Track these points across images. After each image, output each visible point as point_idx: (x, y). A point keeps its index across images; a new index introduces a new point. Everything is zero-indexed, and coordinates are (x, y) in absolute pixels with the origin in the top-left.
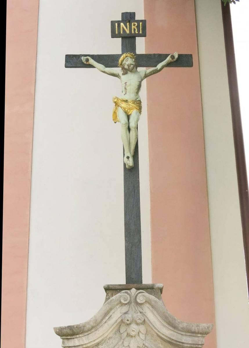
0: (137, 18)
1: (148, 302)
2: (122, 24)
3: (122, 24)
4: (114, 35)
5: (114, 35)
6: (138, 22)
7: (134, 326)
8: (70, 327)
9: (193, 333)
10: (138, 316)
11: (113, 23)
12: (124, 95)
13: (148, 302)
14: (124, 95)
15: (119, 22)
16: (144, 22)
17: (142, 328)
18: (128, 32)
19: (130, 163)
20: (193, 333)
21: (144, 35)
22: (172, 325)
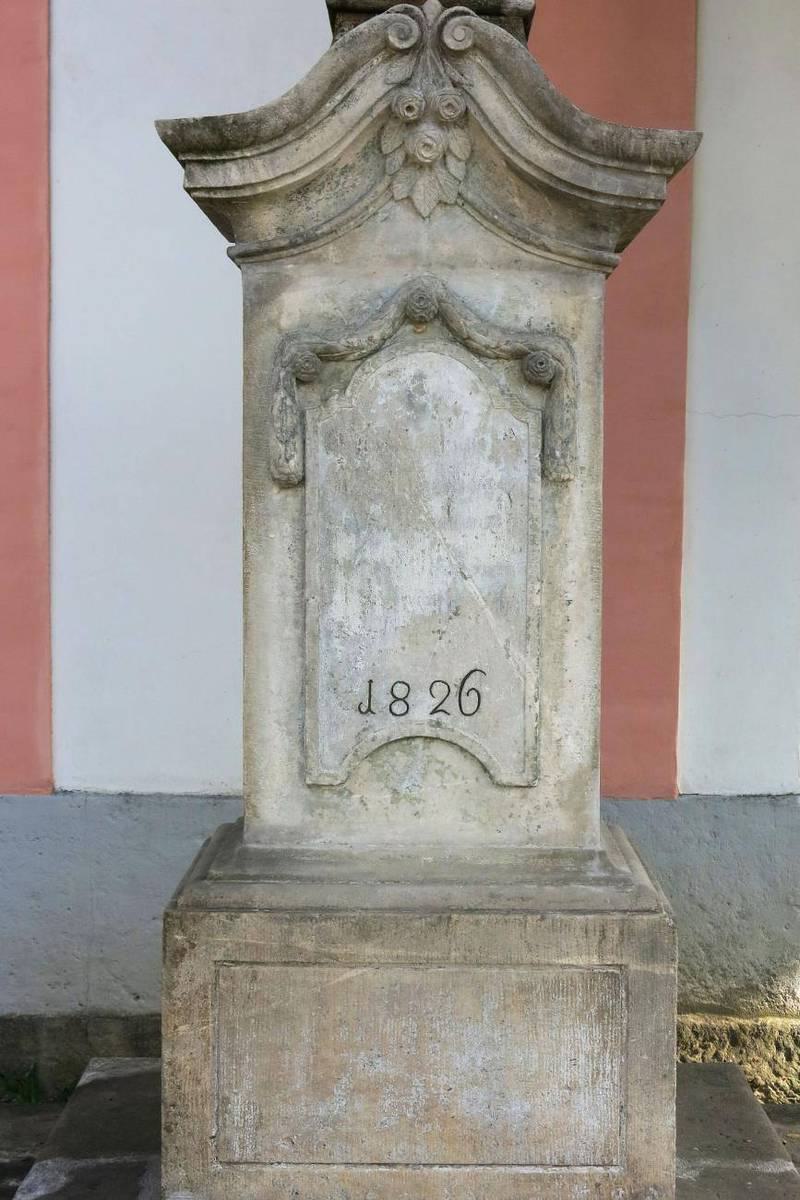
1: (481, 47)
7: (429, 131)
8: (211, 123)
9: (626, 159)
10: (444, 96)
13: (481, 47)
17: (458, 142)
20: (626, 159)
22: (559, 128)
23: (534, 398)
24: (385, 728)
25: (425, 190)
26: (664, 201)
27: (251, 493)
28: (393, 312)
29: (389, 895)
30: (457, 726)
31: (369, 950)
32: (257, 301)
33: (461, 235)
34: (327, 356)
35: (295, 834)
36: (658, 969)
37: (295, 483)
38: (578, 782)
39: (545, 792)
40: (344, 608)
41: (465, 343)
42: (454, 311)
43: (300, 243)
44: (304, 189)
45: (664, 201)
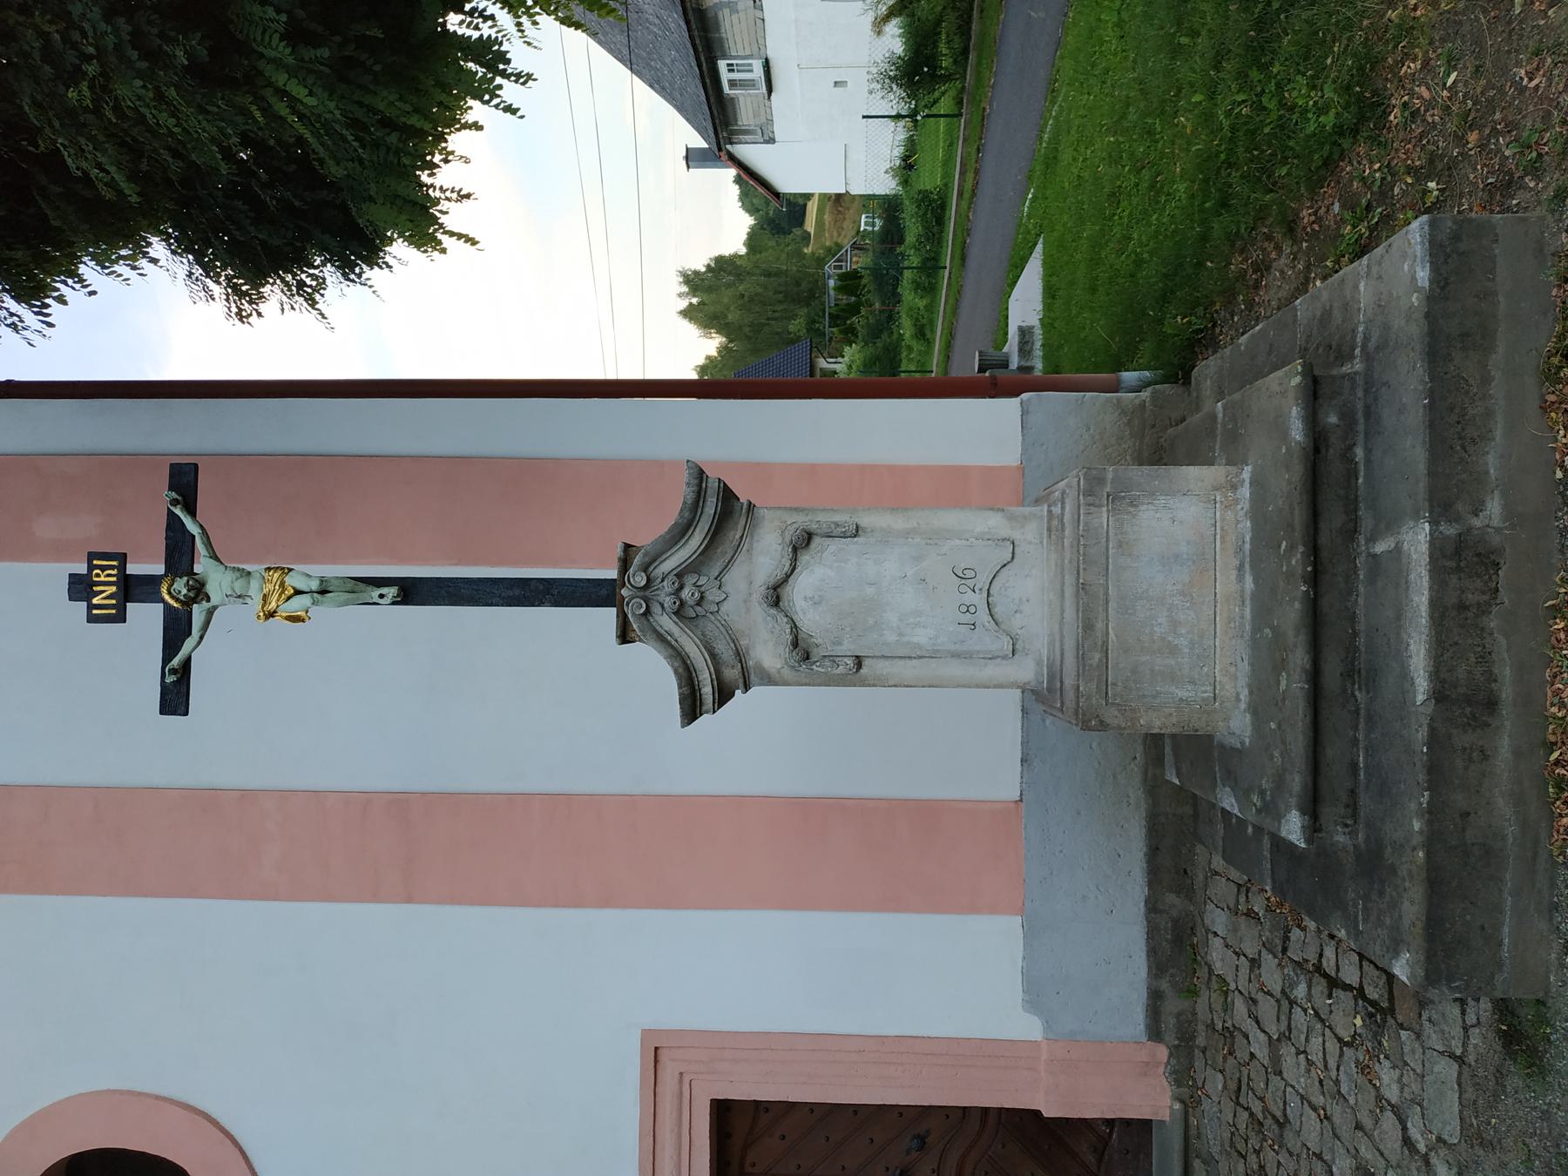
0: (82, 568)
2: (95, 601)
3: (95, 601)
4: (120, 617)
5: (120, 617)
6: (91, 567)
11: (92, 619)
12: (175, 698)
13: (645, 568)
14: (175, 698)
15: (91, 607)
16: (91, 556)
18: (114, 589)
19: (391, 592)
21: (123, 558)
23: (816, 541)
24: (983, 616)
25: (713, 595)
26: (692, 709)
27: (863, 683)
28: (773, 611)
29: (1070, 613)
30: (982, 580)
31: (1100, 625)
32: (769, 680)
33: (736, 579)
34: (795, 644)
35: (1039, 663)
36: (1110, 476)
37: (859, 662)
38: (1012, 518)
39: (1016, 535)
40: (922, 637)
41: (788, 576)
42: (772, 582)
43: (740, 656)
44: (713, 656)
45: (692, 709)
